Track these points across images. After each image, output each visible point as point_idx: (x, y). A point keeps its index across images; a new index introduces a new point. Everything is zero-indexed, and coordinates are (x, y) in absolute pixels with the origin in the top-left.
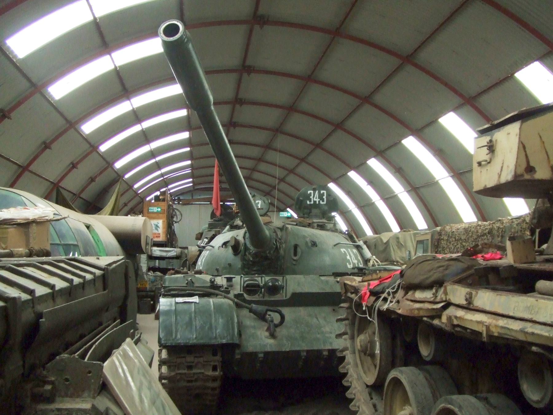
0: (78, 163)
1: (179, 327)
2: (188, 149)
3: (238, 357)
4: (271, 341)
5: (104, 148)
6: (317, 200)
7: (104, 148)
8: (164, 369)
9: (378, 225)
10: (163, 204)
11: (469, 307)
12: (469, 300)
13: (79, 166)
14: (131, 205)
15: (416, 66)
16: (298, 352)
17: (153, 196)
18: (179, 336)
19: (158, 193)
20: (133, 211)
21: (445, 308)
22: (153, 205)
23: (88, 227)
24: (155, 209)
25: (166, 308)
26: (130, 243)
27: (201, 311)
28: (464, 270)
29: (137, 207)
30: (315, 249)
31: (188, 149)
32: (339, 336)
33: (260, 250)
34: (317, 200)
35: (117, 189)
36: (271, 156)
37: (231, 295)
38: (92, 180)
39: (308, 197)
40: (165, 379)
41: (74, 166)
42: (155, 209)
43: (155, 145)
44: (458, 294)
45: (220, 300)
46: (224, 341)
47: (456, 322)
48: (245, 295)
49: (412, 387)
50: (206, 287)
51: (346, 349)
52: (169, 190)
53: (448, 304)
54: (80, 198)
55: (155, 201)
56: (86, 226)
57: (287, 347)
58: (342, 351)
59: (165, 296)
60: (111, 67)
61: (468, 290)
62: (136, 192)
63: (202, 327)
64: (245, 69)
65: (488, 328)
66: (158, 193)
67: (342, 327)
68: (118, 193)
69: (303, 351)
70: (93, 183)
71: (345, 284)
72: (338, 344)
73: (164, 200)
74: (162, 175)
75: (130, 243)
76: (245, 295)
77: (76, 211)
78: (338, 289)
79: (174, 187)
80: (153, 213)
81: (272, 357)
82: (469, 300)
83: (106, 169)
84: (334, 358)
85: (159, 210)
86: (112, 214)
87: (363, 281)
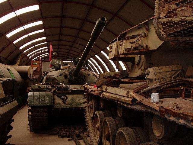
0: (5, 48)
1: (34, 100)
2: (46, 43)
3: (53, 109)
4: (64, 105)
5: (15, 42)
6: (58, 63)
7: (15, 42)
8: (30, 113)
9: (104, 70)
10: (38, 61)
11: (106, 92)
12: (106, 89)
13: (6, 49)
14: (26, 62)
15: (118, 17)
16: (72, 108)
17: (35, 59)
18: (34, 103)
19: (36, 58)
20: (27, 65)
21: (102, 92)
22: (35, 62)
23: (8, 70)
24: (35, 64)
25: (31, 95)
26: (23, 74)
27: (42, 96)
28: (108, 82)
29: (29, 62)
30: (89, 77)
31: (46, 43)
32: (84, 103)
33: (76, 77)
34: (58, 63)
35: (21, 56)
36: (75, 45)
37: (52, 91)
38: (11, 53)
39: (55, 62)
40: (30, 116)
41: (4, 49)
42: (35, 64)
43: (34, 41)
44: (104, 88)
45: (48, 93)
46: (48, 105)
47: (103, 96)
48: (57, 91)
49: (99, 116)
50: (45, 89)
51: (86, 107)
52: (40, 57)
53: (103, 91)
54: (7, 59)
55: (35, 60)
56: (8, 69)
57: (69, 107)
58: (85, 108)
59: (30, 91)
60: (32, 43)
61: (107, 87)
62: (28, 57)
63: (41, 100)
64: (63, 17)
65: (108, 96)
66: (36, 58)
67: (85, 100)
68: (21, 58)
69: (74, 108)
70: (12, 54)
71: (85, 87)
72: (83, 105)
73: (38, 60)
74: (37, 52)
75: (23, 74)
76: (57, 91)
77: (4, 64)
78: (83, 89)
79: (42, 56)
80: (35, 65)
81: (63, 109)
82: (106, 89)
83: (16, 49)
84: (83, 110)
85: (37, 64)
86: (20, 65)
87: (89, 86)
